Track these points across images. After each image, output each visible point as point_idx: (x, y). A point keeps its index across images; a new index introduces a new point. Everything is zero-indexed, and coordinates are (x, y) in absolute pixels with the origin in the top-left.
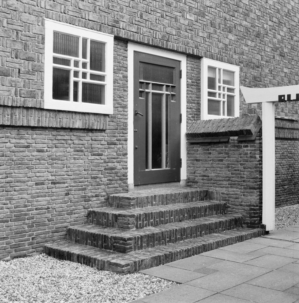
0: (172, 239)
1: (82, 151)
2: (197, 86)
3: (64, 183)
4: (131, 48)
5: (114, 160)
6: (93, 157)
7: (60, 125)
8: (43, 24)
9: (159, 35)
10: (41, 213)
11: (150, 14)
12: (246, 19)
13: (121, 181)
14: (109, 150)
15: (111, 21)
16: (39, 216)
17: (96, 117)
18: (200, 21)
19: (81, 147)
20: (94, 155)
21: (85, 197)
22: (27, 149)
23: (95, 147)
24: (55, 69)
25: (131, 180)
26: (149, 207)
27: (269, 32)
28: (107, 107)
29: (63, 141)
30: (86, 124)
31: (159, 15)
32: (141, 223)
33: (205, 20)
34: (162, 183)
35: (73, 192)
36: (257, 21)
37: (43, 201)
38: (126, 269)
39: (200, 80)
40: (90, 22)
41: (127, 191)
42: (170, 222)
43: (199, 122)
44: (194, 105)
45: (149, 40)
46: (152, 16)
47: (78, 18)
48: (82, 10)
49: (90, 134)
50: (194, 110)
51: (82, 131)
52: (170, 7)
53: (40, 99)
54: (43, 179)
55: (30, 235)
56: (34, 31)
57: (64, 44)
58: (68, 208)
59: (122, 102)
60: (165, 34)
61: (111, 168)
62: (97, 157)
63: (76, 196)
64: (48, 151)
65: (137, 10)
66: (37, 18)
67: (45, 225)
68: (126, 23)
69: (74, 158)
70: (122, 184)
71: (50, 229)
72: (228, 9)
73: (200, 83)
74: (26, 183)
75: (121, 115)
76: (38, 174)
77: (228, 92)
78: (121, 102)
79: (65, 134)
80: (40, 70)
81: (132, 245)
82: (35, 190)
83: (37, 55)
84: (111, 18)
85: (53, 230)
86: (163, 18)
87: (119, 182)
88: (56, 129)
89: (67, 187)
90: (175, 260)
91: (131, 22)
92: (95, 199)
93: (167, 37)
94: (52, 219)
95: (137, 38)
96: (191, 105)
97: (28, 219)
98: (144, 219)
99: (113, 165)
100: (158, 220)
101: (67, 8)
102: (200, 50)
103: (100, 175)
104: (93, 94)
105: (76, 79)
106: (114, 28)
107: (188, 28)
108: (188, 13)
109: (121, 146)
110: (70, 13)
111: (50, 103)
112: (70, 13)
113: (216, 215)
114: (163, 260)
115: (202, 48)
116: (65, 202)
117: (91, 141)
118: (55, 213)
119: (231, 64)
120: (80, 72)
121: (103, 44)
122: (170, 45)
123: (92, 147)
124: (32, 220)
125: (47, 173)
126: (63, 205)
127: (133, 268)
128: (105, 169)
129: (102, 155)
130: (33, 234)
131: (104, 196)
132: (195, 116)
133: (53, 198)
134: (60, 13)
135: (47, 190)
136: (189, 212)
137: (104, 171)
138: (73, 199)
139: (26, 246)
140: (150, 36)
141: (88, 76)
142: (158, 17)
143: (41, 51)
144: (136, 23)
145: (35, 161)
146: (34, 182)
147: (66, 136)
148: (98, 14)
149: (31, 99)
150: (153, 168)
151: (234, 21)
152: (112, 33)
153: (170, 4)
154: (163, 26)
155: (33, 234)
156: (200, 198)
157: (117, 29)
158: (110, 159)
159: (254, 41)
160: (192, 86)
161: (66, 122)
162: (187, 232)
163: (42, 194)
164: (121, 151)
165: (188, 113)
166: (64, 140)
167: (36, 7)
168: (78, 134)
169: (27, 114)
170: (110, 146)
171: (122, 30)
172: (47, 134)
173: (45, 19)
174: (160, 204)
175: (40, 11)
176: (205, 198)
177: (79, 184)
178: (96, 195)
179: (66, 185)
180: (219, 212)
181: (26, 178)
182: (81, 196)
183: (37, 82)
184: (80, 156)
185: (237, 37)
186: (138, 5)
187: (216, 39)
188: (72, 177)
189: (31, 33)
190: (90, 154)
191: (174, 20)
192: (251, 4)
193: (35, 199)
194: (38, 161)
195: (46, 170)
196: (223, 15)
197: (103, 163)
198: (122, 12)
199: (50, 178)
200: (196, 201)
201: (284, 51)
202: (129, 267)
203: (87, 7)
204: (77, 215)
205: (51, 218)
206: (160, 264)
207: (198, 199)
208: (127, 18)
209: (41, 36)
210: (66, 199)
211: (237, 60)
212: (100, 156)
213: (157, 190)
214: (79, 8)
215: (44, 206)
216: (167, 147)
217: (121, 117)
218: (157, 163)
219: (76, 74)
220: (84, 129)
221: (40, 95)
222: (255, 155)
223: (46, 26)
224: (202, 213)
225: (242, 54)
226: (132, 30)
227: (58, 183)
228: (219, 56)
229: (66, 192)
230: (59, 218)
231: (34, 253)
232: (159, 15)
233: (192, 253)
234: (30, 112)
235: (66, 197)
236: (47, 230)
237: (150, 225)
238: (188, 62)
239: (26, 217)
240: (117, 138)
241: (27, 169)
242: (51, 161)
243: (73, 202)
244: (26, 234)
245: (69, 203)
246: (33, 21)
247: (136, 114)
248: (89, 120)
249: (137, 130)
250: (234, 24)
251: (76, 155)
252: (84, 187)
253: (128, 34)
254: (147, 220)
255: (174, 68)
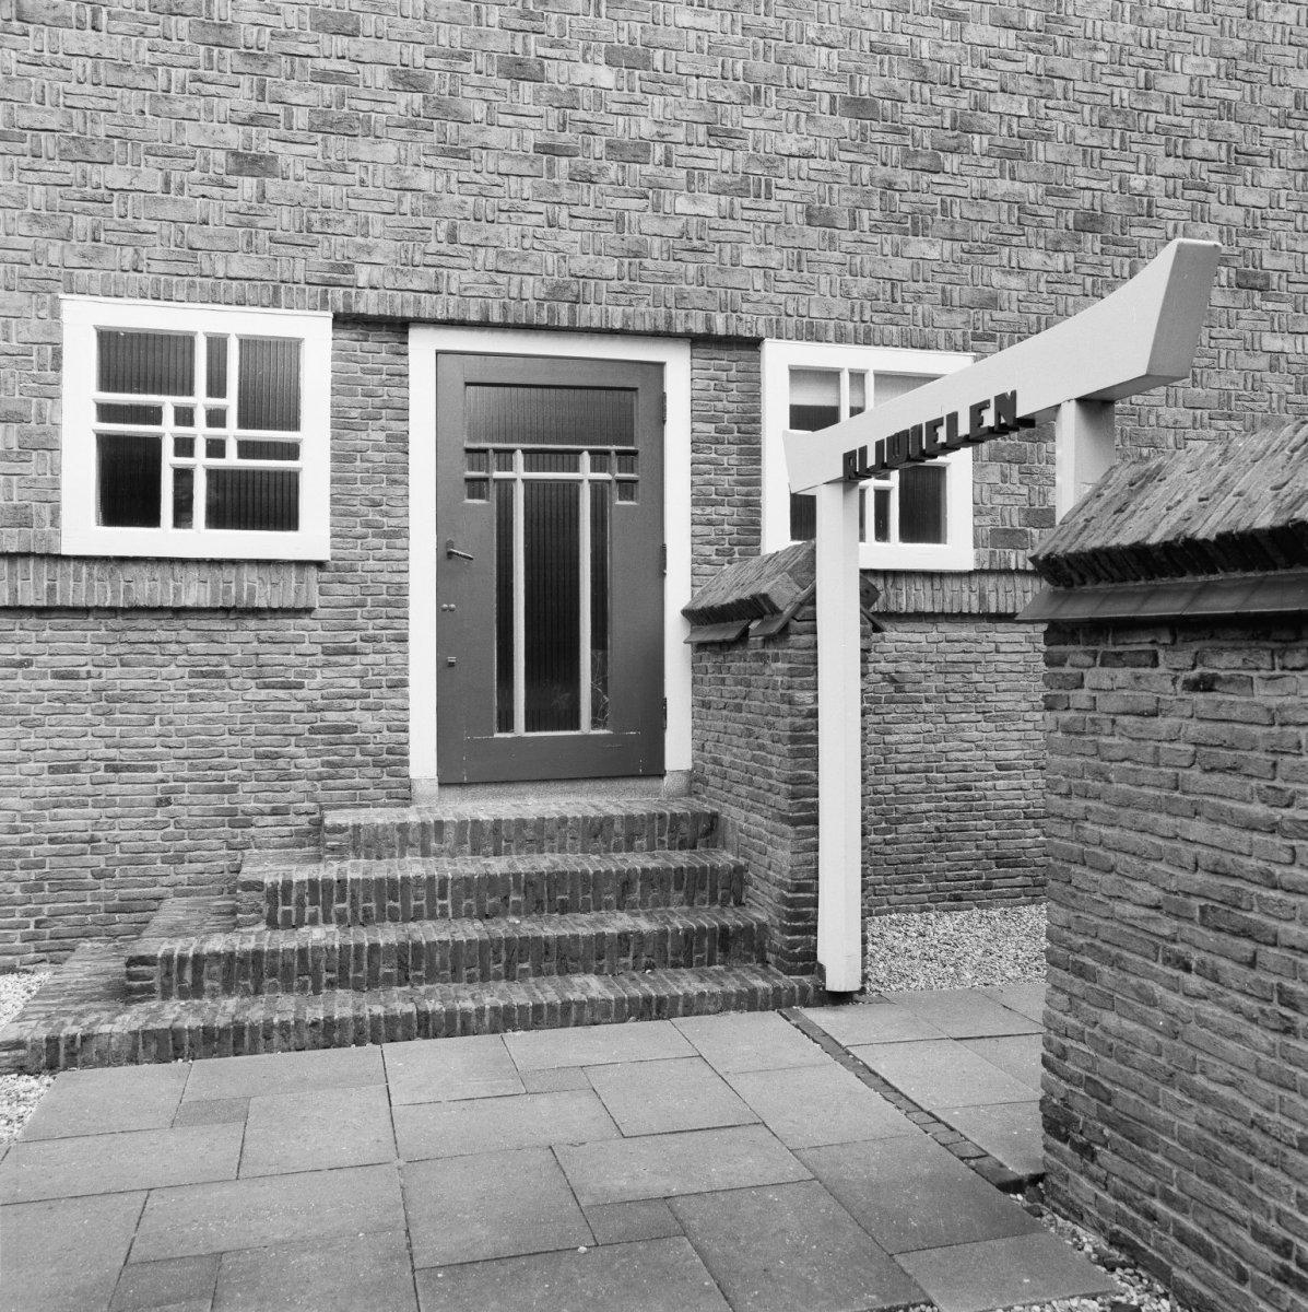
0: (351, 975)
1: (221, 675)
2: (746, 443)
3: (152, 769)
4: (423, 346)
5: (350, 703)
6: (263, 694)
7: (126, 599)
8: (55, 313)
9: (533, 289)
10: (69, 852)
11: (493, 222)
12: (1012, 170)
13: (378, 770)
14: (327, 672)
15: (321, 268)
16: (61, 861)
17: (264, 572)
18: (747, 214)
19: (215, 663)
20: (267, 686)
21: (231, 813)
22: (20, 671)
23: (270, 662)
24: (106, 443)
25: (423, 761)
26: (408, 858)
27: (1163, 201)
28: (312, 536)
29: (147, 647)
30: (227, 592)
31: (541, 219)
32: (290, 911)
33: (773, 205)
34: (577, 779)
35: (185, 797)
36: (1081, 171)
37: (76, 820)
38: (6, 1058)
39: (757, 420)
40: (235, 283)
41: (407, 801)
42: (432, 917)
43: (754, 560)
44: (725, 510)
45: (486, 311)
46: (502, 229)
47: (187, 279)
48: (199, 253)
49: (252, 623)
50: (726, 527)
51: (219, 615)
52: (592, 186)
53: (48, 528)
54: (74, 755)
55: (28, 914)
56: (26, 336)
57: (135, 362)
58: (168, 843)
59: (385, 520)
60: (568, 278)
61: (334, 727)
62: (281, 693)
63: (195, 810)
64: (94, 674)
65: (435, 220)
66: (34, 297)
67: (81, 888)
68: (382, 268)
69: (190, 695)
70: (385, 778)
71: (99, 900)
72: (908, 150)
73: (757, 432)
74: (17, 766)
75: (379, 560)
76: (58, 742)
77: (528, 467)
78: (378, 518)
79: (154, 624)
81: (156, 981)
82: (46, 787)
83: (34, 405)
84: (321, 260)
85: (110, 903)
86: (555, 230)
87: (371, 771)
88: (113, 611)
89: (162, 781)
90: (253, 1051)
91: (404, 261)
92: (270, 820)
93: (568, 291)
94: (107, 873)
95: (431, 307)
96: (709, 510)
97: (22, 868)
98: (307, 899)
99: (343, 718)
100: (373, 905)
101: (144, 256)
102: (744, 316)
103: (292, 749)
104: (258, 500)
105: (183, 461)
106: (330, 289)
107: (678, 244)
108: (685, 192)
109: (379, 658)
110: (157, 267)
112: (157, 267)
113: (686, 908)
114: (191, 1045)
115: (760, 306)
116: (156, 826)
117: (255, 644)
118: (118, 855)
119: (923, 348)
120: (197, 433)
121: (292, 346)
122: (589, 315)
123: (261, 662)
124: (37, 871)
125: (90, 738)
126: (148, 834)
127: (40, 1057)
128: (313, 731)
129: (300, 686)
130: (39, 912)
131: (307, 813)
132: (736, 549)
133: (110, 812)
134: (118, 273)
135: (89, 788)
136: (530, 890)
137: (307, 735)
138: (185, 817)
139: (17, 943)
140: (492, 295)
141: (232, 449)
142: (531, 229)
143: (49, 390)
144: (429, 260)
145: (46, 703)
146: (46, 765)
147: (161, 631)
148: (266, 256)
149: (16, 530)
150: (527, 730)
151: (937, 189)
152: (324, 304)
153: (591, 175)
154: (556, 256)
155: (39, 912)
156: (671, 839)
157: (348, 289)
158: (334, 700)
159: (1064, 247)
160: (718, 446)
161: (146, 588)
162: (433, 958)
163: (71, 798)
164: (379, 674)
165: (696, 541)
166: (152, 642)
167: (33, 266)
168: (204, 624)
169: (10, 574)
170: (333, 659)
171: (367, 291)
172: (90, 626)
173: (61, 296)
174: (462, 852)
175: (44, 275)
176: (700, 841)
177: (208, 772)
178: (274, 808)
179: (159, 774)
180: (706, 895)
181: (17, 751)
182: (215, 810)
183: (35, 480)
184: (213, 688)
185: (957, 245)
186: (439, 203)
187: (833, 269)
188: (180, 753)
189: (15, 343)
190: (252, 683)
191: (610, 227)
192: (1047, 108)
193: (46, 813)
194: (57, 704)
195: (89, 729)
196: (876, 174)
197: (301, 711)
198: (366, 235)
199: (102, 752)
200: (651, 848)
201: (1265, 265)
202: (21, 1052)
203: (221, 238)
204: (199, 866)
205: (102, 870)
206: (176, 1058)
207: (662, 842)
208: (385, 249)
209: (50, 348)
210: (158, 817)
211: (959, 332)
212: (294, 691)
213: (480, 803)
214: (191, 248)
215: (77, 834)
217: (377, 568)
218: (553, 707)
219: (184, 447)
220: (226, 610)
221: (47, 516)
222: (790, 691)
223: (65, 317)
224: (607, 893)
225: (992, 302)
226: (410, 286)
227: (129, 768)
228: (850, 326)
229: (160, 795)
230: (132, 870)
231: (42, 965)
232: (541, 219)
233: (351, 1035)
234: (20, 564)
235: (159, 809)
236: (89, 904)
237: (334, 919)
238: (699, 363)
239: (17, 862)
240: (363, 633)
241: (18, 728)
242: (103, 703)
243: (183, 825)
244: (13, 911)
245: (171, 829)
246: (19, 309)
247: (447, 556)
248: (239, 582)
249: (453, 606)
250: (939, 198)
251: (195, 686)
252: (227, 782)
253: (392, 302)
254: (317, 903)
255: (635, 389)
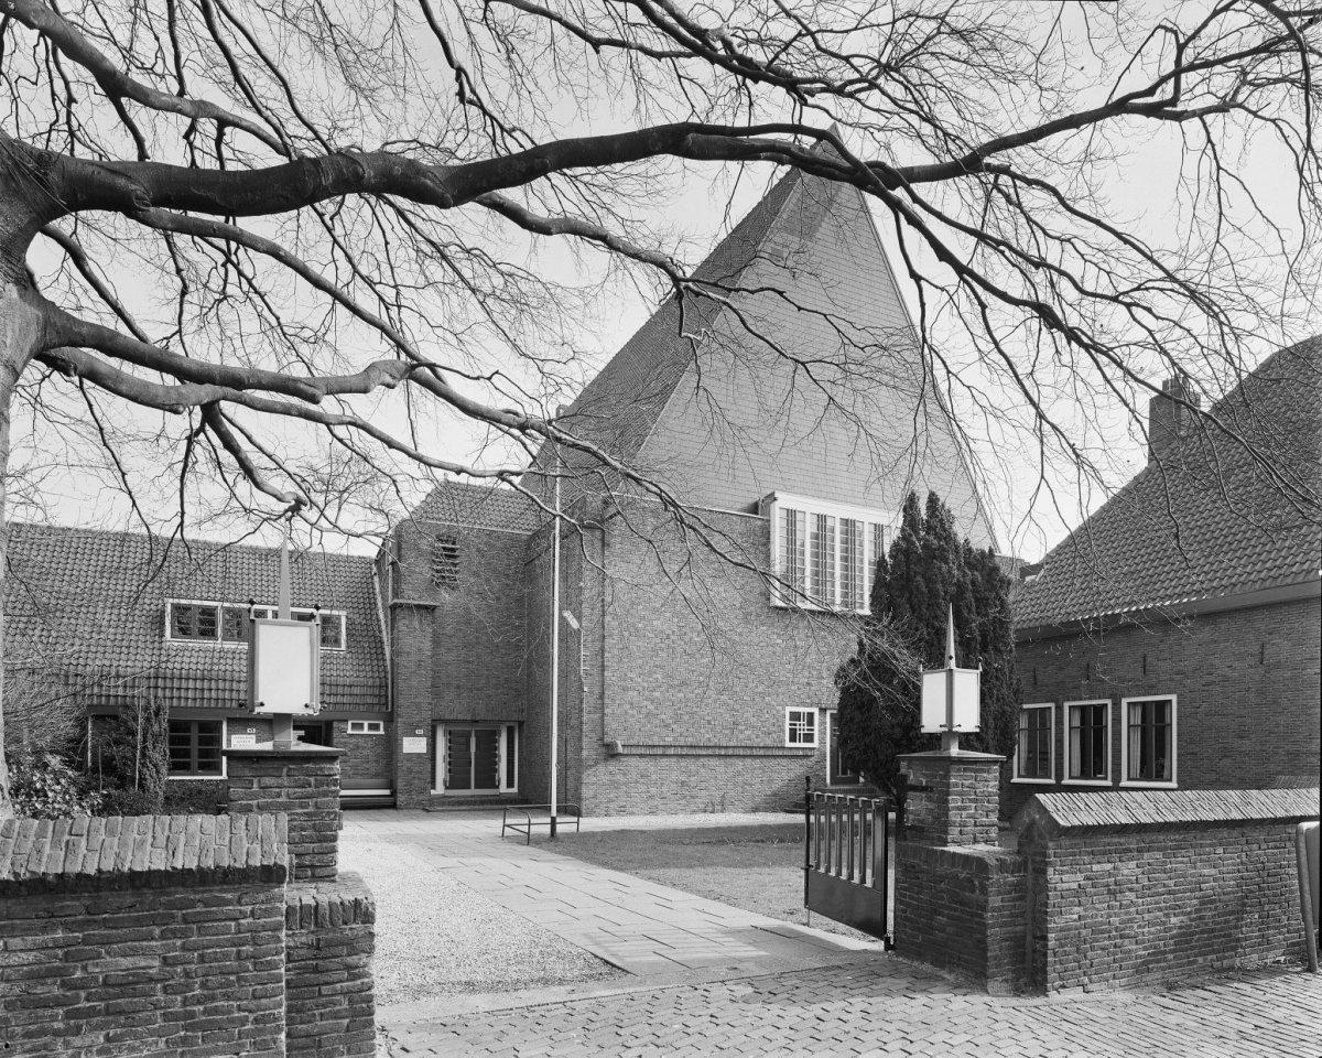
25: (828, 781)
28: (815, 744)
57: (795, 716)
80: (784, 731)
104: (809, 738)
111: (788, 744)
120: (802, 727)
161: (795, 753)
216: (523, 166)
